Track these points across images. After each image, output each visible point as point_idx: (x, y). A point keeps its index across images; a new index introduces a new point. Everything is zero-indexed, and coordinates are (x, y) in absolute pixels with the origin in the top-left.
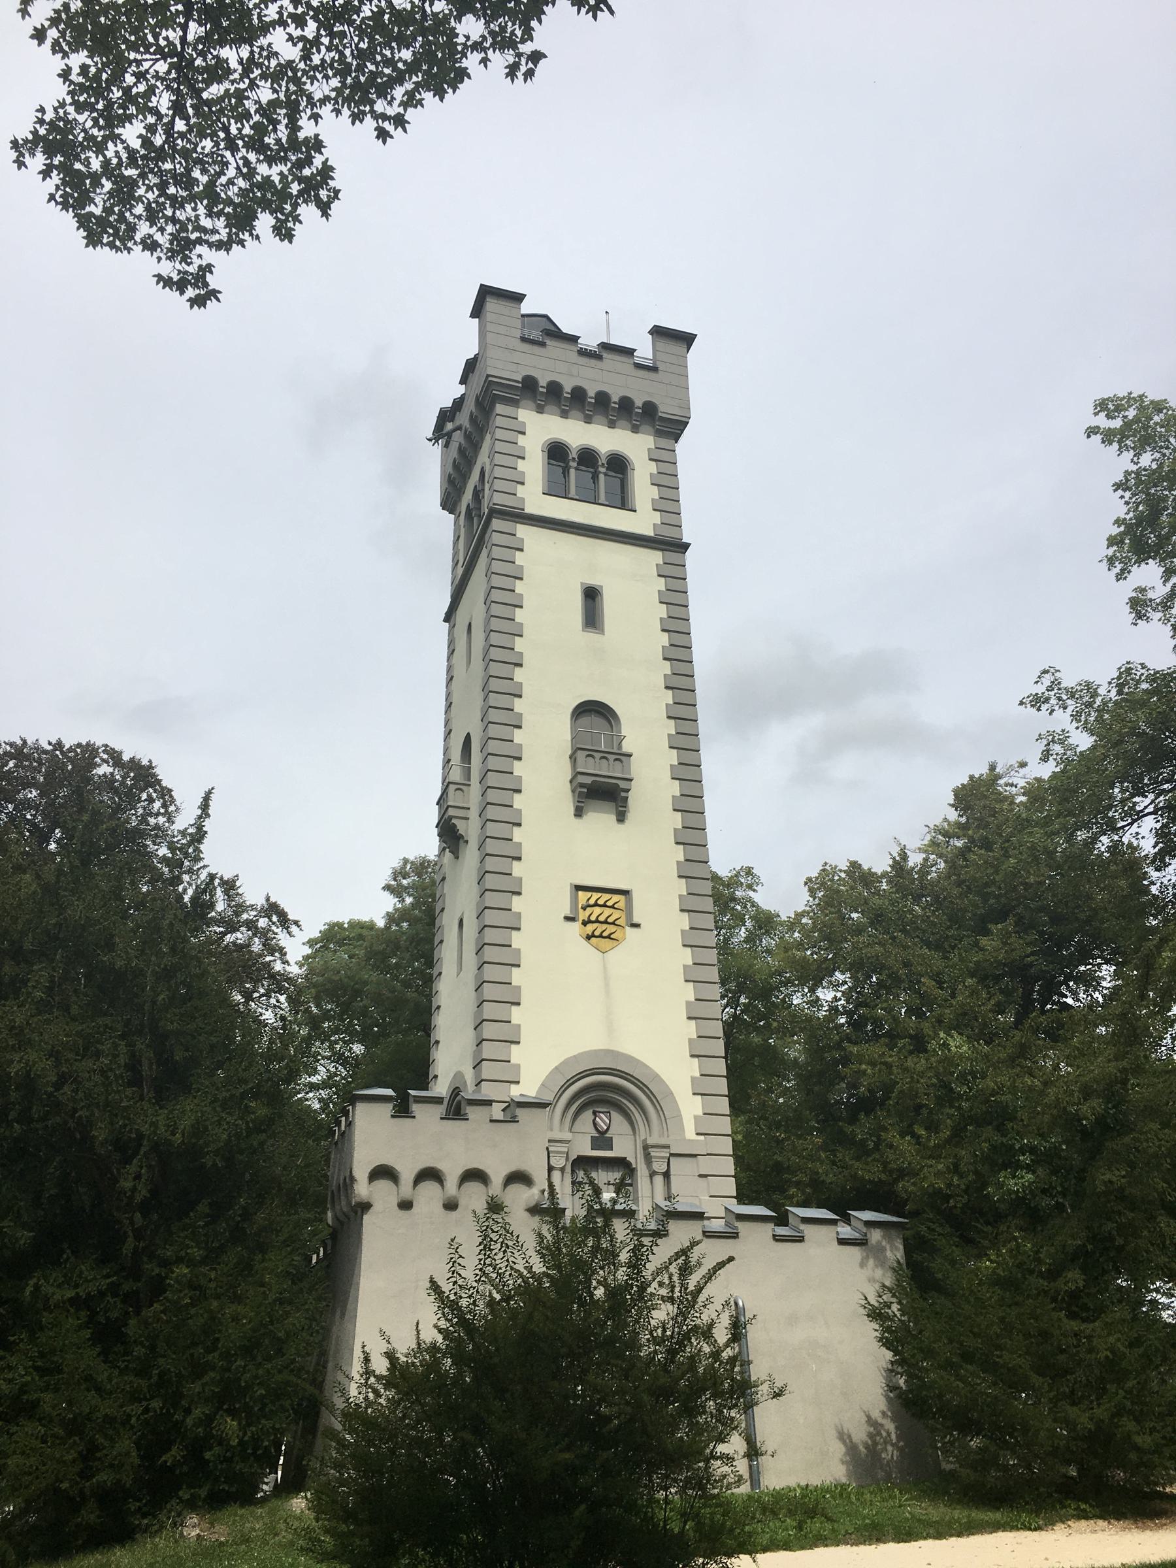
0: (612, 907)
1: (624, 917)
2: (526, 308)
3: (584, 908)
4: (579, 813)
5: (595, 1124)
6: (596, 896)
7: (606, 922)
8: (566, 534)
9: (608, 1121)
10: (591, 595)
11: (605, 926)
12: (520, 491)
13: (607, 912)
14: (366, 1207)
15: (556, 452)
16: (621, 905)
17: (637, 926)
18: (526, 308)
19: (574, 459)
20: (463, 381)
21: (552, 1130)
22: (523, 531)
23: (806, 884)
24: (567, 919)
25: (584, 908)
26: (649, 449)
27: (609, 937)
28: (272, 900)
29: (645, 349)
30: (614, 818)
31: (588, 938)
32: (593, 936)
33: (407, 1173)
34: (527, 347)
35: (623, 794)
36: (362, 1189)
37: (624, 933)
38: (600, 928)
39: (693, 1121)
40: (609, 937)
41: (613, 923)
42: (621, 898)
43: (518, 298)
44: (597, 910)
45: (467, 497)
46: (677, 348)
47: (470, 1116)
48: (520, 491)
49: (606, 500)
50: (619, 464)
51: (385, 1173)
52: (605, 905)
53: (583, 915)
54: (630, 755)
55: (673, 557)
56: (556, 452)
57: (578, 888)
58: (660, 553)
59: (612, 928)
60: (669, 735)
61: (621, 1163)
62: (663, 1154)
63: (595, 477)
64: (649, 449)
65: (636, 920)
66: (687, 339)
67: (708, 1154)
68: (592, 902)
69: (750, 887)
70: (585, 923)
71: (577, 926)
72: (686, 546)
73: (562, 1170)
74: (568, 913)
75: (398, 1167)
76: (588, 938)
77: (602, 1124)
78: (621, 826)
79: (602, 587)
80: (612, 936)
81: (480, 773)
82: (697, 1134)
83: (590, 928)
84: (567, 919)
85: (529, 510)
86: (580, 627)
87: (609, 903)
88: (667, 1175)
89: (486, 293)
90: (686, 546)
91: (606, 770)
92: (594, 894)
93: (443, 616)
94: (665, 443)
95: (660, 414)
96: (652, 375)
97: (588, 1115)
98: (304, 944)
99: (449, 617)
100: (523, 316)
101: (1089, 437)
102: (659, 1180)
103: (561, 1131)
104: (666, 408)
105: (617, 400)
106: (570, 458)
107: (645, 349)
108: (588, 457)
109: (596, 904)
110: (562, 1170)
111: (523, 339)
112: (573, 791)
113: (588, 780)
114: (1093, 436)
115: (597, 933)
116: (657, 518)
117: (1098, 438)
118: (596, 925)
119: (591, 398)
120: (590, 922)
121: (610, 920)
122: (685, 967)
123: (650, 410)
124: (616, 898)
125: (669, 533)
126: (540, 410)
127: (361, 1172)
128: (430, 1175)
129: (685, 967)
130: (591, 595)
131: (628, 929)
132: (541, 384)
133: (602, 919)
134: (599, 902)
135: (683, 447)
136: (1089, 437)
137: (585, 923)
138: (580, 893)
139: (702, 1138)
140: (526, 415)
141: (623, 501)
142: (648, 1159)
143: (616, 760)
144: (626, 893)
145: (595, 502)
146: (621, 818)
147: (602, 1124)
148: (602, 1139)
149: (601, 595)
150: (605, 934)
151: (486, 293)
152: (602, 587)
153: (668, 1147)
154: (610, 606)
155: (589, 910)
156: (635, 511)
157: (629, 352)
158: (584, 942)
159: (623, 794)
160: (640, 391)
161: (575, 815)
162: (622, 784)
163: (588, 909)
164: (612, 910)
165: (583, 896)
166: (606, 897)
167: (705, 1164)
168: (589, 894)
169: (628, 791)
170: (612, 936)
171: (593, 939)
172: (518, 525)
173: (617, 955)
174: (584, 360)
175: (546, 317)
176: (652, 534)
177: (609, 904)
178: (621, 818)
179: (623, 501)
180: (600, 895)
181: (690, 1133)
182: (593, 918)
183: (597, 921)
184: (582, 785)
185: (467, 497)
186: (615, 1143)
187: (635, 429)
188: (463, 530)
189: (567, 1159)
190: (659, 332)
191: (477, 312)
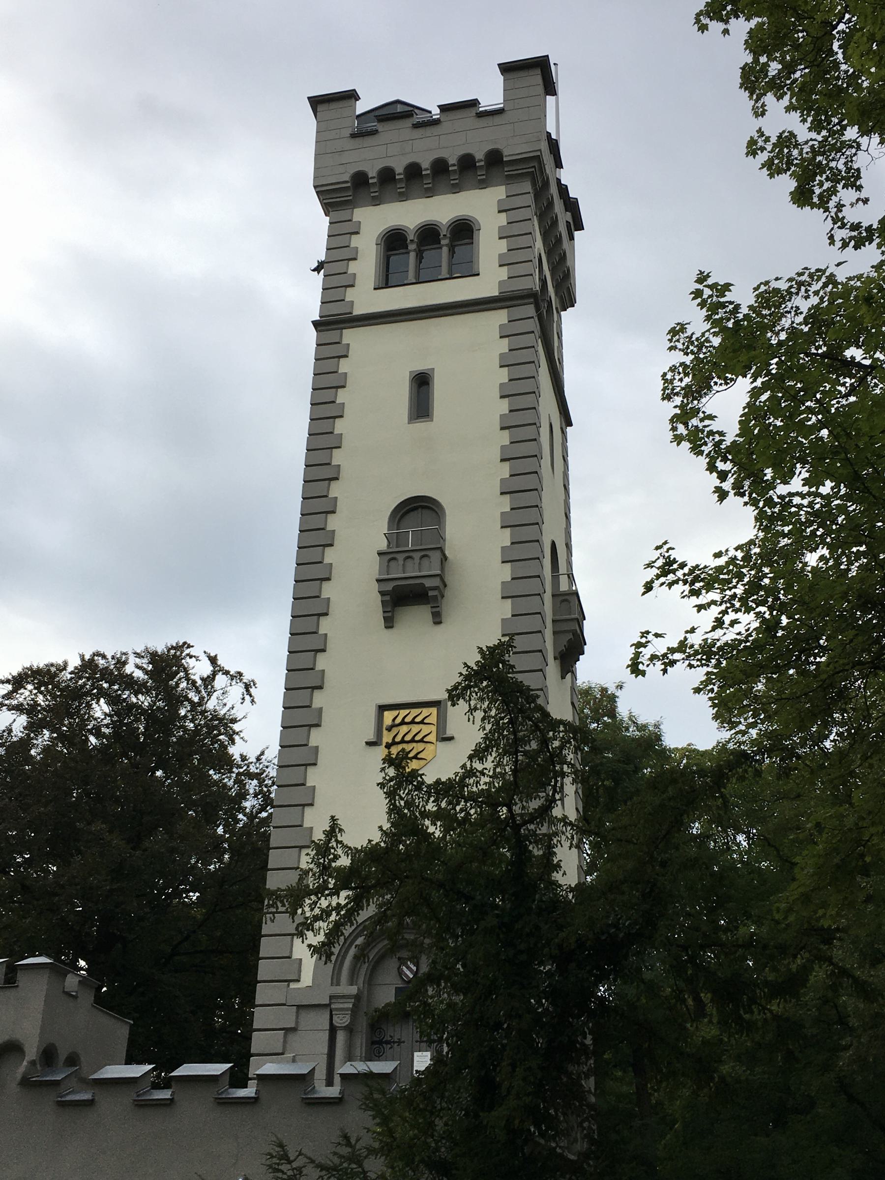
0: (422, 722)
3: (389, 729)
4: (389, 623)
5: (400, 973)
6: (403, 713)
8: (462, 316)
12: (350, 295)
13: (415, 729)
16: (433, 719)
17: (451, 739)
21: (338, 984)
24: (370, 744)
25: (389, 729)
34: (359, 141)
41: (422, 741)
42: (434, 711)
43: (352, 96)
44: (404, 729)
48: (350, 295)
52: (413, 722)
53: (387, 738)
57: (382, 708)
59: (421, 746)
62: (346, 1006)
65: (449, 733)
68: (398, 721)
74: (371, 737)
77: (408, 973)
80: (419, 756)
84: (370, 744)
85: (358, 311)
86: (406, 421)
92: (402, 711)
97: (392, 964)
105: (374, 175)
109: (403, 723)
113: (389, 587)
119: (399, 174)
124: (425, 712)
131: (440, 745)
132: (450, 163)
137: (388, 746)
138: (386, 713)
146: (437, 619)
147: (408, 973)
155: (395, 731)
161: (386, 627)
165: (388, 717)
166: (415, 712)
168: (395, 713)
170: (419, 756)
175: (398, 102)
178: (437, 619)
180: (407, 711)
182: (398, 739)
187: (483, 184)
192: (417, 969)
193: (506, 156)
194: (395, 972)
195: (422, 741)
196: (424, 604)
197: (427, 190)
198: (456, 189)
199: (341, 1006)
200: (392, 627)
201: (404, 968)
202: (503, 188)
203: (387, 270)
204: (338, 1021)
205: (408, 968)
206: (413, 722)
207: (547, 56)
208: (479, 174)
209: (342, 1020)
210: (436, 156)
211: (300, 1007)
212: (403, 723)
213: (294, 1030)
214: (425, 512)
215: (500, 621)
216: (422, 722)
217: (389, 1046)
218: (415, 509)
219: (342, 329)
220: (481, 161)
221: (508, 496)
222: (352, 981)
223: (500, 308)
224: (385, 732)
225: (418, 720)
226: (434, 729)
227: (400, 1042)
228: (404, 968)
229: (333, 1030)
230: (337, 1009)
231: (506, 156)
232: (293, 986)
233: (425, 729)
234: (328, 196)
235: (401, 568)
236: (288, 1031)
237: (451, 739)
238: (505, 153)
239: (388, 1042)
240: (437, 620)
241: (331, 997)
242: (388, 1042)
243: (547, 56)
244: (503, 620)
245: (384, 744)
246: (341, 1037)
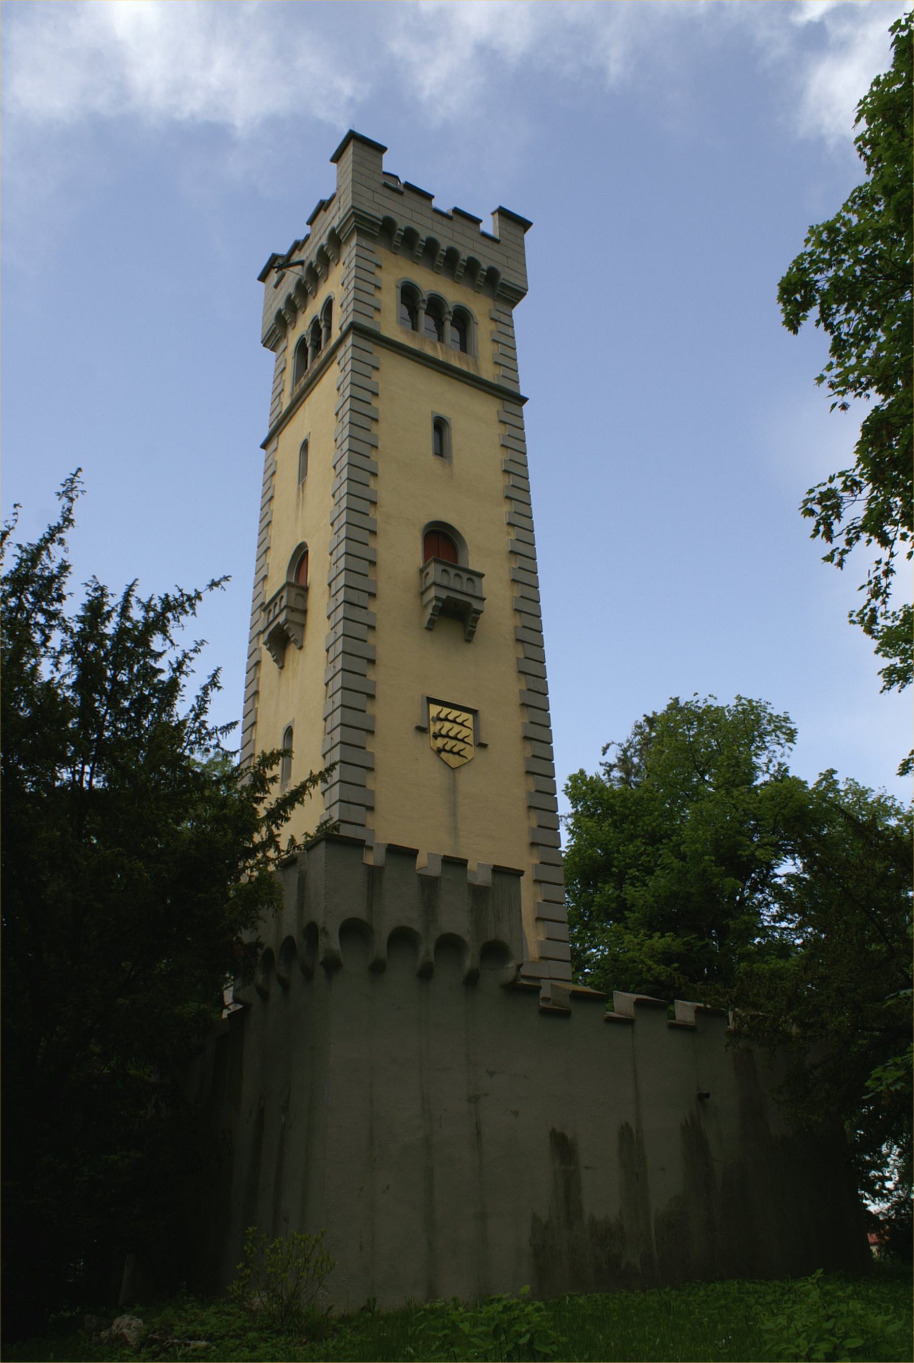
0: (462, 724)
1: (472, 735)
6: (446, 710)
7: (455, 738)
10: (440, 425)
11: (454, 742)
15: (409, 293)
16: (469, 723)
19: (424, 301)
20: (311, 222)
27: (458, 753)
29: (489, 226)
38: (451, 743)
40: (458, 753)
41: (462, 740)
44: (448, 725)
45: (302, 327)
52: (454, 721)
57: (431, 701)
70: (436, 736)
72: (524, 400)
79: (450, 419)
81: (255, 581)
83: (440, 742)
87: (459, 720)
90: (524, 400)
94: (504, 308)
96: (495, 246)
104: (506, 276)
107: (489, 226)
108: (436, 305)
109: (446, 719)
113: (444, 594)
118: (446, 740)
123: (492, 275)
124: (465, 716)
130: (440, 425)
133: (452, 734)
134: (457, 720)
135: (518, 312)
143: (469, 579)
144: (474, 712)
150: (455, 750)
154: (457, 438)
157: (477, 221)
160: (487, 258)
162: (476, 605)
164: (461, 728)
165: (434, 710)
170: (461, 753)
178: (469, 637)
183: (447, 736)
185: (302, 327)
190: (503, 213)
238: (502, 277)
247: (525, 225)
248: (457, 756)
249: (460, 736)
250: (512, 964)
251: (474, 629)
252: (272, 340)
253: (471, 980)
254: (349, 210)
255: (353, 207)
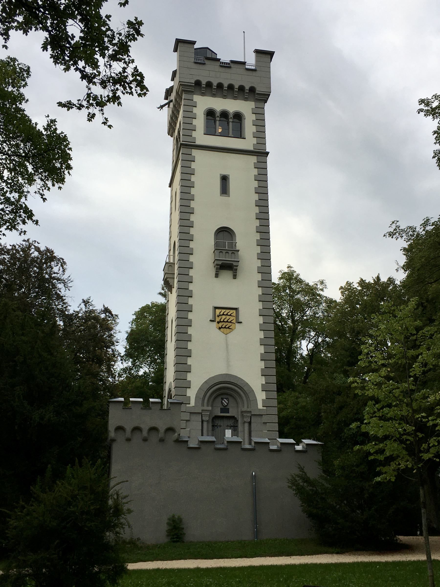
0: (230, 315)
2: (196, 46)
3: (218, 316)
4: (217, 276)
5: (222, 403)
6: (223, 311)
7: (227, 322)
9: (227, 402)
10: (225, 179)
12: (194, 134)
13: (228, 317)
14: (113, 440)
15: (210, 113)
16: (234, 314)
17: (241, 322)
18: (196, 46)
19: (218, 116)
20: (173, 79)
21: (203, 406)
22: (195, 153)
23: (340, 289)
25: (218, 316)
26: (252, 109)
27: (228, 328)
28: (106, 306)
30: (232, 277)
31: (220, 328)
32: (222, 327)
33: (129, 428)
35: (235, 268)
36: (112, 434)
37: (235, 326)
38: (225, 324)
39: (261, 401)
40: (228, 328)
41: (230, 322)
42: (234, 311)
43: (194, 43)
44: (224, 317)
46: (266, 58)
47: (152, 408)
48: (194, 134)
49: (233, 134)
50: (238, 116)
51: (120, 429)
52: (227, 315)
53: (218, 319)
54: (238, 251)
55: (261, 159)
56: (210, 113)
57: (216, 308)
58: (255, 157)
59: (230, 324)
60: (257, 240)
61: (233, 417)
62: (207, 413)
63: (228, 123)
64: (252, 109)
65: (240, 320)
66: (271, 54)
67: (267, 415)
68: (222, 313)
69: (322, 290)
70: (218, 323)
71: (215, 324)
72: (267, 153)
73: (208, 421)
74: (211, 318)
75: (125, 427)
76: (220, 328)
77: (225, 403)
78: (234, 280)
80: (230, 328)
82: (263, 406)
83: (220, 325)
85: (198, 142)
88: (250, 423)
89: (178, 42)
90: (267, 153)
91: (228, 258)
92: (223, 310)
93: (168, 185)
94: (260, 105)
95: (257, 92)
96: (254, 73)
97: (219, 399)
98: (133, 315)
99: (170, 186)
100: (195, 49)
101: (419, 113)
102: (246, 425)
103: (207, 406)
104: (260, 89)
106: (216, 116)
108: (224, 114)
109: (223, 314)
110: (208, 421)
111: (195, 63)
112: (215, 267)
113: (220, 263)
114: (421, 113)
115: (223, 326)
116: (255, 141)
117: (422, 114)
118: (223, 323)
119: (226, 87)
120: (221, 322)
121: (229, 321)
122: (261, 339)
123: (252, 90)
124: (232, 311)
125: (260, 147)
126: (203, 94)
127: (111, 427)
128: (137, 429)
129: (261, 339)
130: (225, 179)
133: (225, 320)
134: (225, 314)
136: (419, 113)
137: (218, 323)
138: (217, 310)
139: (265, 408)
140: (197, 98)
141: (240, 135)
142: (243, 416)
144: (236, 309)
145: (270, 95)
146: (235, 277)
147: (225, 403)
148: (225, 409)
149: (229, 179)
151: (178, 42)
152: (229, 175)
153: (251, 412)
155: (220, 317)
156: (245, 139)
158: (218, 330)
159: (235, 268)
162: (235, 264)
163: (220, 316)
165: (218, 311)
166: (228, 311)
167: (265, 419)
168: (220, 310)
169: (237, 266)
170: (230, 328)
171: (222, 329)
172: (193, 150)
173: (232, 336)
174: (223, 70)
176: (251, 148)
177: (229, 314)
178: (235, 277)
179: (240, 135)
180: (225, 310)
181: (260, 406)
182: (222, 320)
183: (223, 321)
184: (217, 265)
186: (230, 410)
187: (246, 99)
188: (175, 146)
189: (209, 417)
190: (258, 52)
191: (175, 50)
192: (222, 401)
193: (258, 91)
194: (220, 402)
195: (230, 322)
196: (230, 270)
197: (225, 95)
198: (225, 97)
199: (205, 413)
200: (218, 277)
201: (223, 401)
202: (253, 103)
203: (241, 132)
204: (204, 418)
205: (225, 401)
206: (227, 315)
207: (176, 39)
208: (224, 92)
209: (206, 418)
210: (253, 85)
211: (190, 413)
212: (223, 314)
213: (189, 420)
214: (226, 233)
215: (257, 282)
216: (230, 315)
217: (216, 427)
218: (226, 231)
219: (192, 149)
220: (204, 85)
221: (259, 233)
222: (208, 406)
223: (216, 151)
224: (217, 317)
225: (229, 314)
226: (235, 318)
227: (220, 426)
228: (223, 401)
229: (202, 421)
230: (204, 415)
231: (258, 91)
232: (188, 405)
233: (232, 318)
234: (183, 87)
235: (224, 256)
236: (187, 421)
237: (241, 322)
238: (257, 90)
239: (216, 426)
240: (234, 277)
241: (202, 410)
242: (216, 426)
243: (176, 39)
244: (258, 281)
245: (217, 322)
246: (205, 424)
247: (271, 54)
248: (228, 329)
249: (227, 327)
250: (176, 434)
251: (236, 274)
252: (169, 135)
253: (162, 440)
254: (179, 83)
255: (180, 82)
